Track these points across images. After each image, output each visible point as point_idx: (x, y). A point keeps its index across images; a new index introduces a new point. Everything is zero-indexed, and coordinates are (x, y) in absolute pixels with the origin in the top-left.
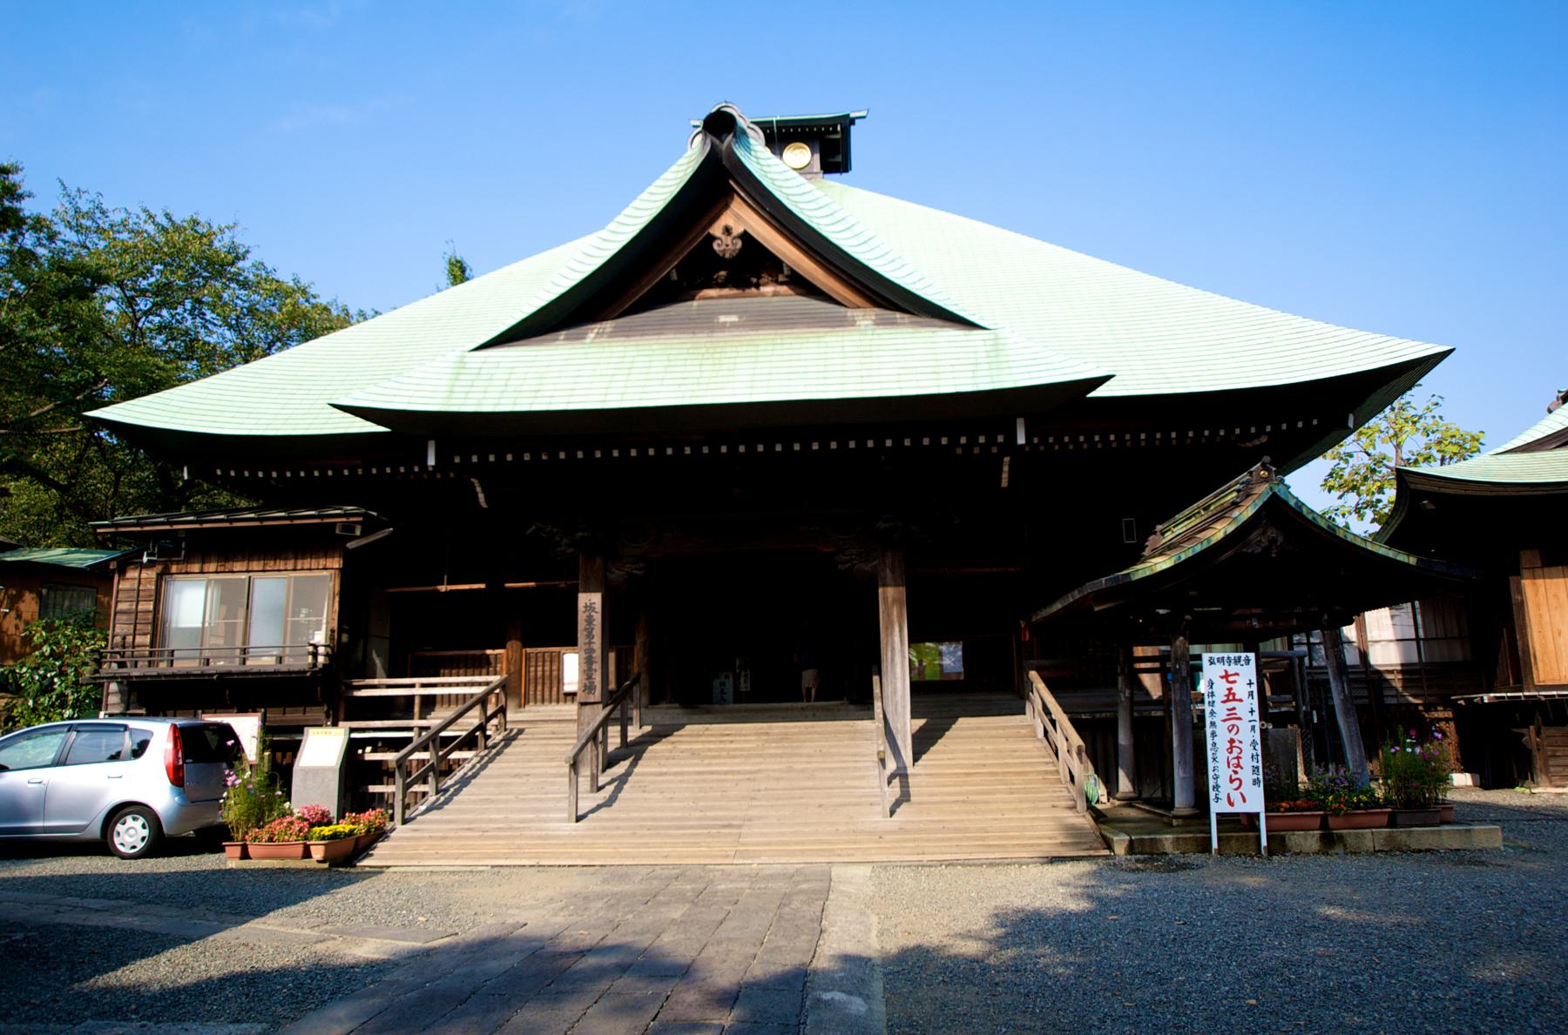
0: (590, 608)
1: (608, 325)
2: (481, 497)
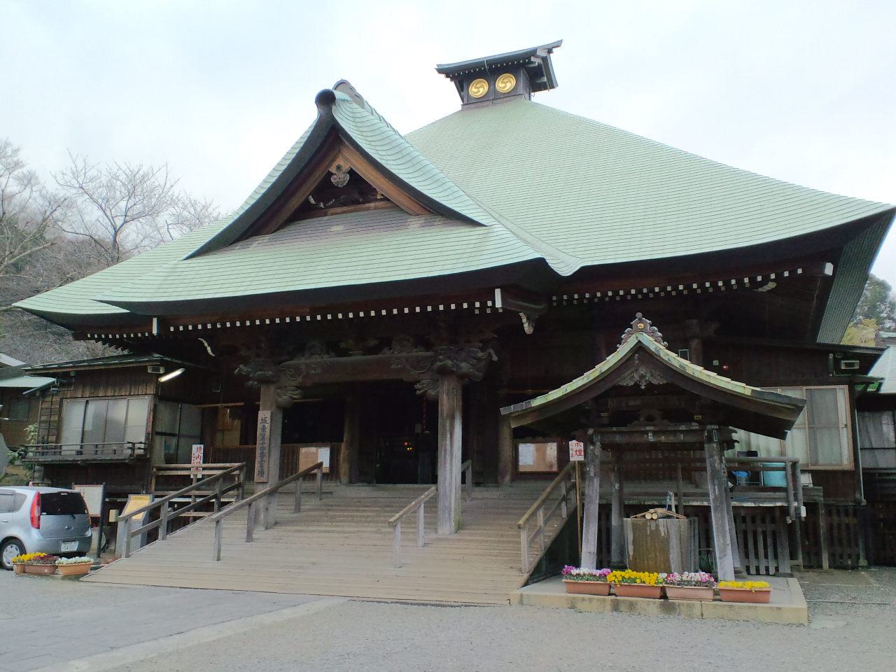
0: (264, 421)
1: (267, 237)
2: (209, 349)
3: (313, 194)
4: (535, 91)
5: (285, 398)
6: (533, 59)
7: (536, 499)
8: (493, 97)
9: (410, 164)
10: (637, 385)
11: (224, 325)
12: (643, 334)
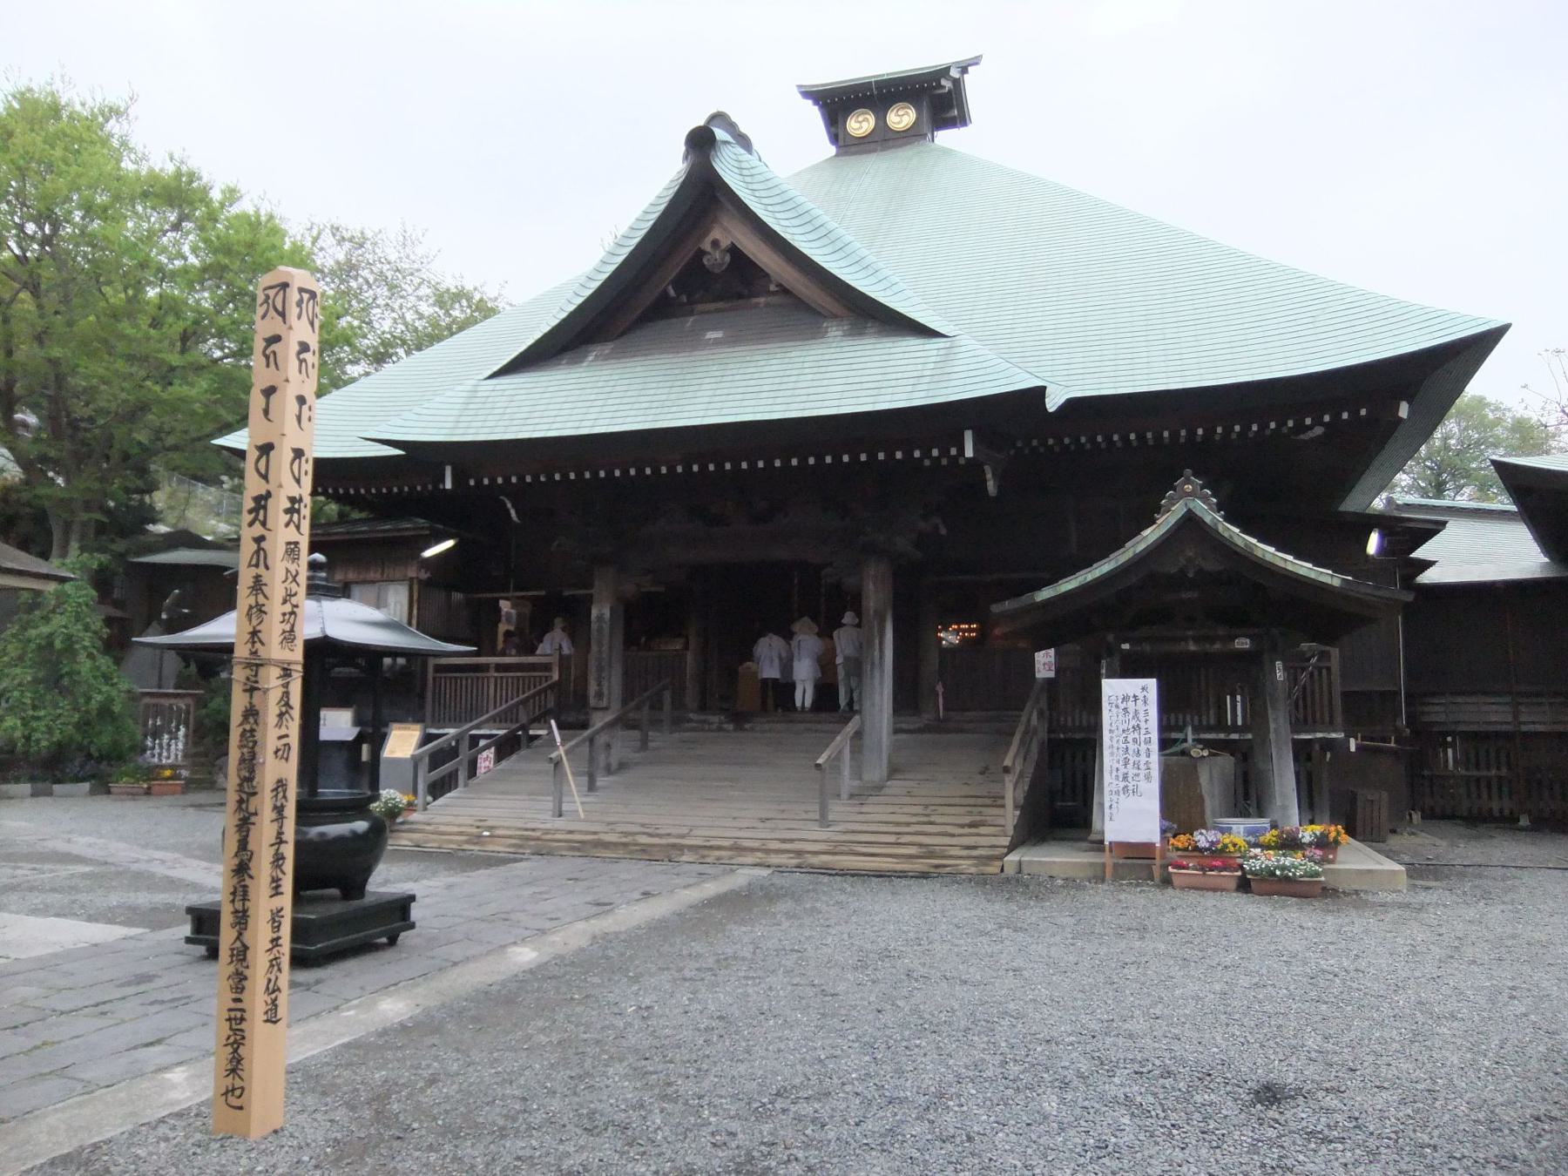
1: (607, 348)
2: (513, 512)
3: (675, 283)
4: (939, 128)
5: (629, 589)
6: (943, 82)
7: (1013, 734)
8: (883, 139)
9: (825, 241)
10: (1182, 572)
11: (550, 477)
12: (1191, 501)
